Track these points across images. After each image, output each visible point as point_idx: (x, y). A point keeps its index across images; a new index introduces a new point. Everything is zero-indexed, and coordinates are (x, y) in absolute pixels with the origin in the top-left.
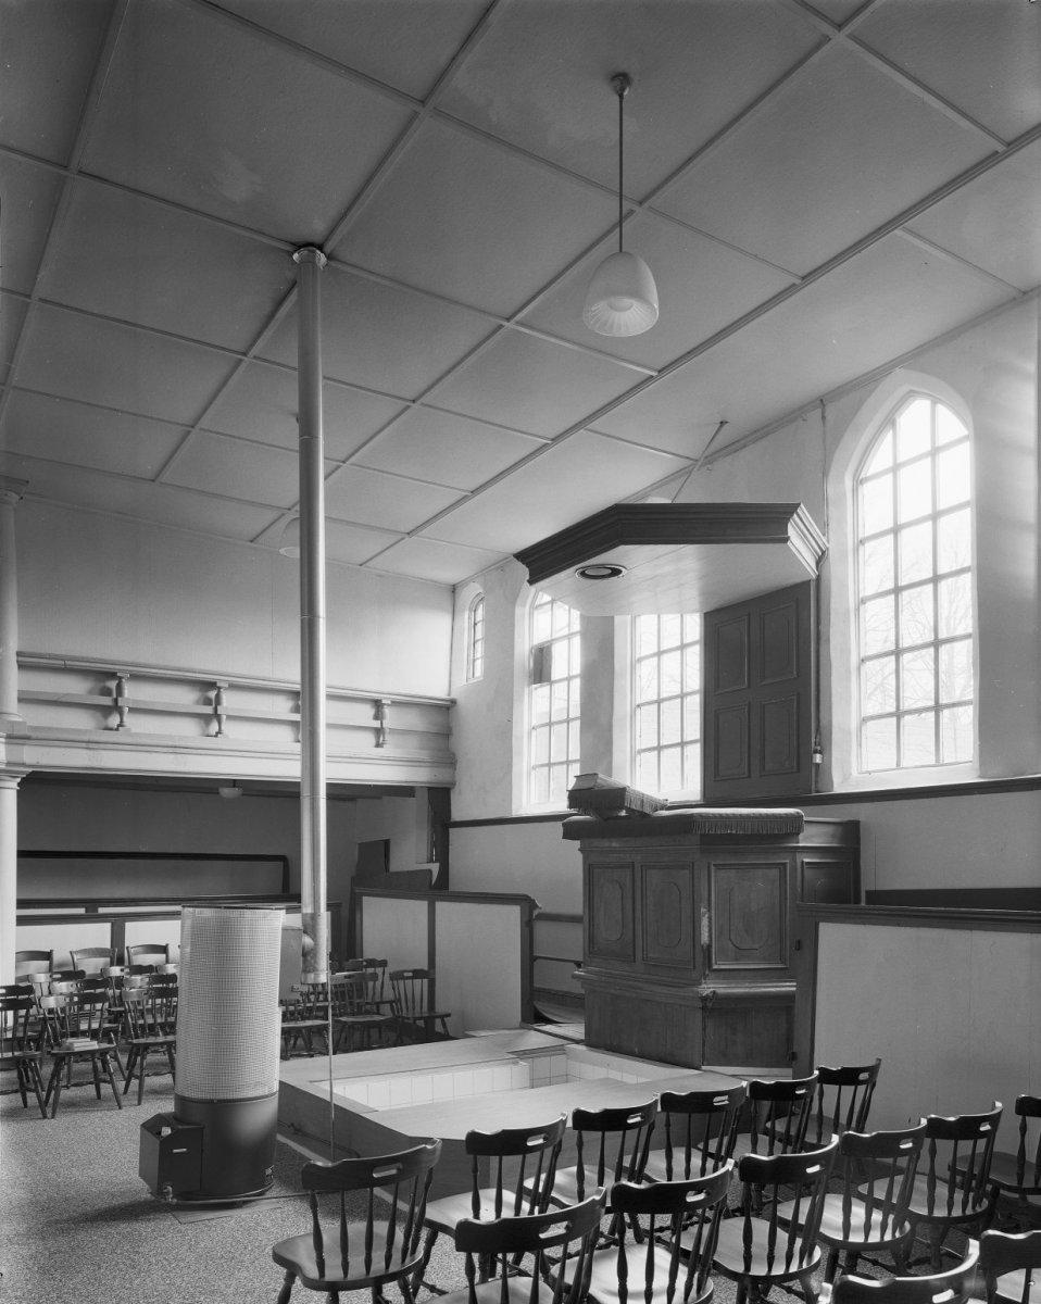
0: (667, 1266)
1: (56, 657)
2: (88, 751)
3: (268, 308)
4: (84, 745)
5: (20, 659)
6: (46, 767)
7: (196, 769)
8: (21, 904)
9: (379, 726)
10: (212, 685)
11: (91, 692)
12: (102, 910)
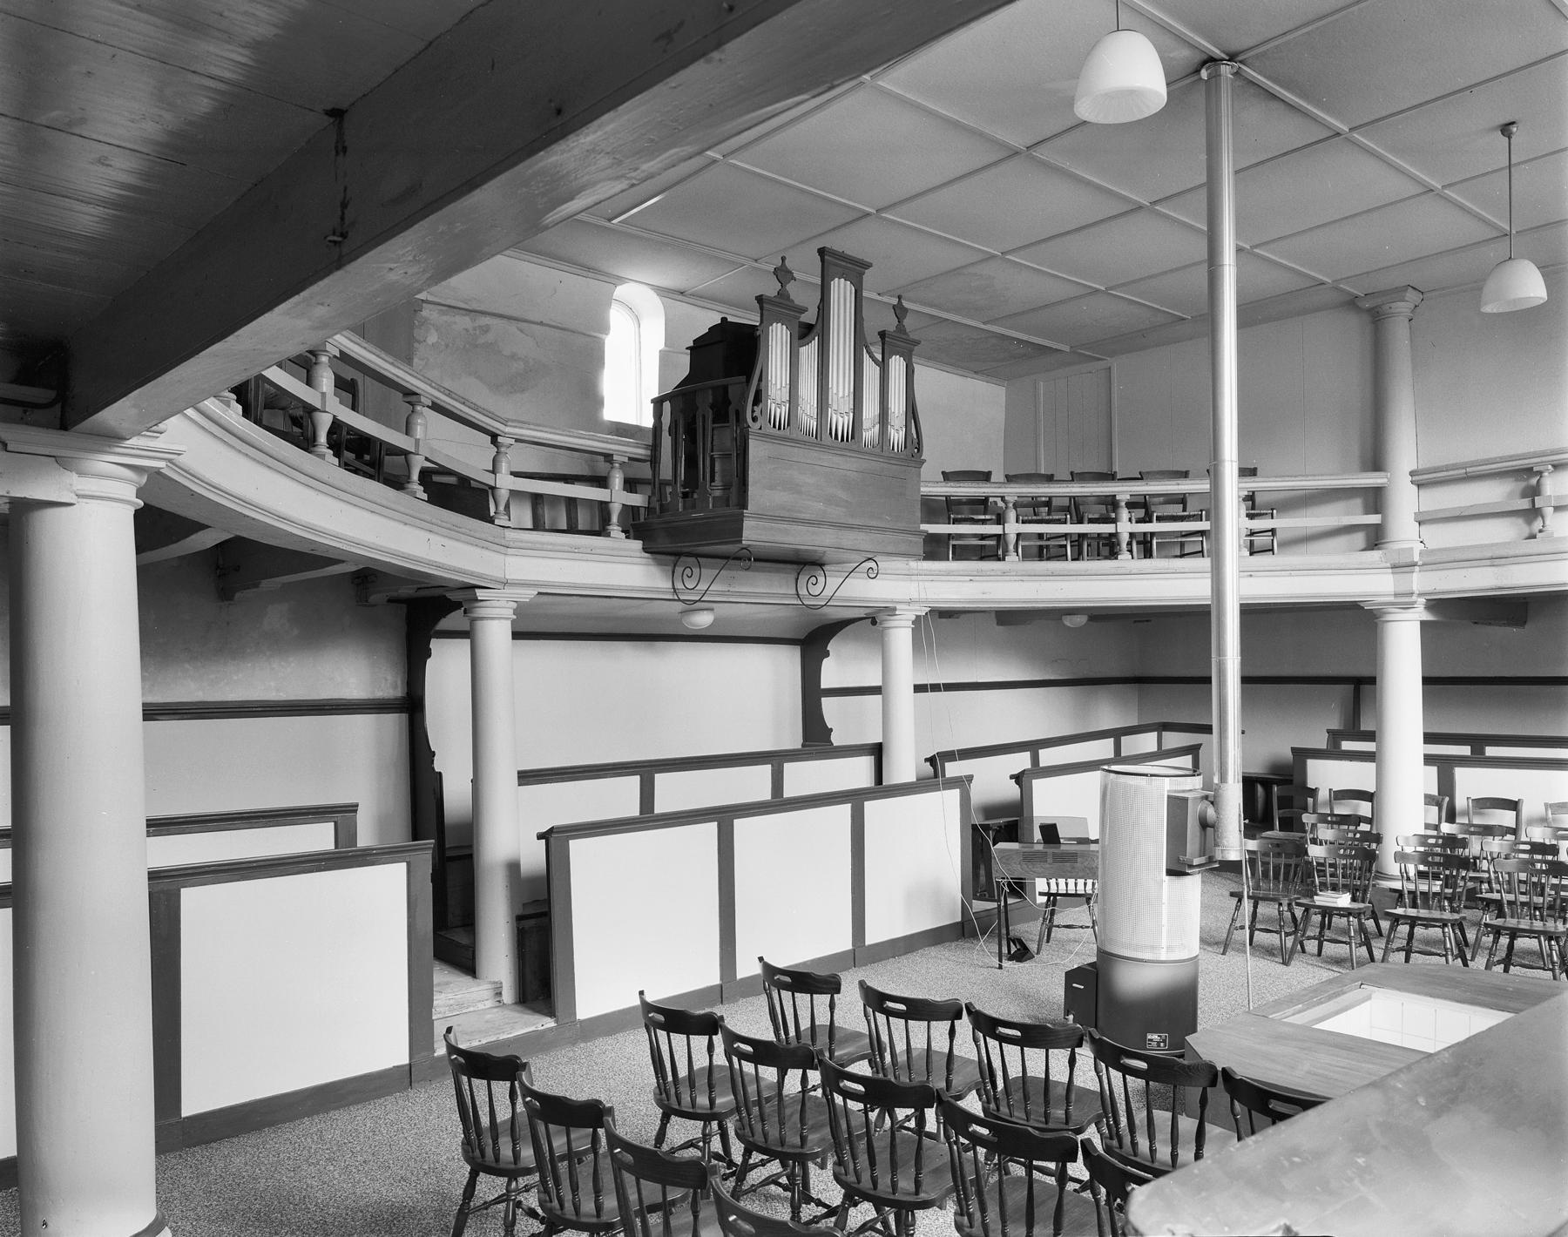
0: (467, 1080)
1: (1455, 467)
2: (1493, 568)
3: (1184, 75)
4: (1488, 562)
5: (1415, 478)
6: (1443, 593)
7: (1522, 582)
8: (1430, 738)
9: (1001, 532)
10: (1529, 471)
11: (1510, 495)
12: (1491, 751)
